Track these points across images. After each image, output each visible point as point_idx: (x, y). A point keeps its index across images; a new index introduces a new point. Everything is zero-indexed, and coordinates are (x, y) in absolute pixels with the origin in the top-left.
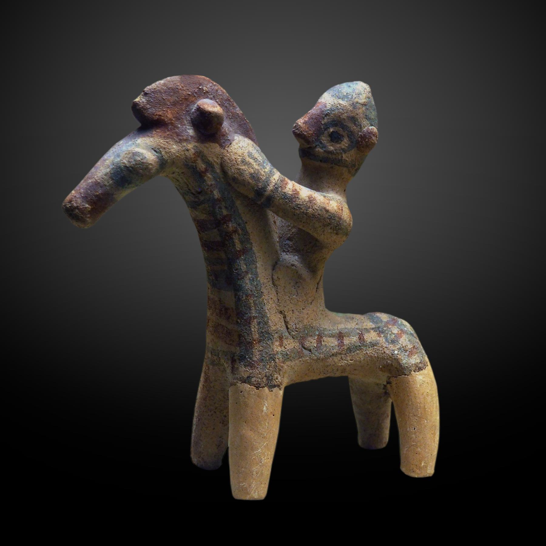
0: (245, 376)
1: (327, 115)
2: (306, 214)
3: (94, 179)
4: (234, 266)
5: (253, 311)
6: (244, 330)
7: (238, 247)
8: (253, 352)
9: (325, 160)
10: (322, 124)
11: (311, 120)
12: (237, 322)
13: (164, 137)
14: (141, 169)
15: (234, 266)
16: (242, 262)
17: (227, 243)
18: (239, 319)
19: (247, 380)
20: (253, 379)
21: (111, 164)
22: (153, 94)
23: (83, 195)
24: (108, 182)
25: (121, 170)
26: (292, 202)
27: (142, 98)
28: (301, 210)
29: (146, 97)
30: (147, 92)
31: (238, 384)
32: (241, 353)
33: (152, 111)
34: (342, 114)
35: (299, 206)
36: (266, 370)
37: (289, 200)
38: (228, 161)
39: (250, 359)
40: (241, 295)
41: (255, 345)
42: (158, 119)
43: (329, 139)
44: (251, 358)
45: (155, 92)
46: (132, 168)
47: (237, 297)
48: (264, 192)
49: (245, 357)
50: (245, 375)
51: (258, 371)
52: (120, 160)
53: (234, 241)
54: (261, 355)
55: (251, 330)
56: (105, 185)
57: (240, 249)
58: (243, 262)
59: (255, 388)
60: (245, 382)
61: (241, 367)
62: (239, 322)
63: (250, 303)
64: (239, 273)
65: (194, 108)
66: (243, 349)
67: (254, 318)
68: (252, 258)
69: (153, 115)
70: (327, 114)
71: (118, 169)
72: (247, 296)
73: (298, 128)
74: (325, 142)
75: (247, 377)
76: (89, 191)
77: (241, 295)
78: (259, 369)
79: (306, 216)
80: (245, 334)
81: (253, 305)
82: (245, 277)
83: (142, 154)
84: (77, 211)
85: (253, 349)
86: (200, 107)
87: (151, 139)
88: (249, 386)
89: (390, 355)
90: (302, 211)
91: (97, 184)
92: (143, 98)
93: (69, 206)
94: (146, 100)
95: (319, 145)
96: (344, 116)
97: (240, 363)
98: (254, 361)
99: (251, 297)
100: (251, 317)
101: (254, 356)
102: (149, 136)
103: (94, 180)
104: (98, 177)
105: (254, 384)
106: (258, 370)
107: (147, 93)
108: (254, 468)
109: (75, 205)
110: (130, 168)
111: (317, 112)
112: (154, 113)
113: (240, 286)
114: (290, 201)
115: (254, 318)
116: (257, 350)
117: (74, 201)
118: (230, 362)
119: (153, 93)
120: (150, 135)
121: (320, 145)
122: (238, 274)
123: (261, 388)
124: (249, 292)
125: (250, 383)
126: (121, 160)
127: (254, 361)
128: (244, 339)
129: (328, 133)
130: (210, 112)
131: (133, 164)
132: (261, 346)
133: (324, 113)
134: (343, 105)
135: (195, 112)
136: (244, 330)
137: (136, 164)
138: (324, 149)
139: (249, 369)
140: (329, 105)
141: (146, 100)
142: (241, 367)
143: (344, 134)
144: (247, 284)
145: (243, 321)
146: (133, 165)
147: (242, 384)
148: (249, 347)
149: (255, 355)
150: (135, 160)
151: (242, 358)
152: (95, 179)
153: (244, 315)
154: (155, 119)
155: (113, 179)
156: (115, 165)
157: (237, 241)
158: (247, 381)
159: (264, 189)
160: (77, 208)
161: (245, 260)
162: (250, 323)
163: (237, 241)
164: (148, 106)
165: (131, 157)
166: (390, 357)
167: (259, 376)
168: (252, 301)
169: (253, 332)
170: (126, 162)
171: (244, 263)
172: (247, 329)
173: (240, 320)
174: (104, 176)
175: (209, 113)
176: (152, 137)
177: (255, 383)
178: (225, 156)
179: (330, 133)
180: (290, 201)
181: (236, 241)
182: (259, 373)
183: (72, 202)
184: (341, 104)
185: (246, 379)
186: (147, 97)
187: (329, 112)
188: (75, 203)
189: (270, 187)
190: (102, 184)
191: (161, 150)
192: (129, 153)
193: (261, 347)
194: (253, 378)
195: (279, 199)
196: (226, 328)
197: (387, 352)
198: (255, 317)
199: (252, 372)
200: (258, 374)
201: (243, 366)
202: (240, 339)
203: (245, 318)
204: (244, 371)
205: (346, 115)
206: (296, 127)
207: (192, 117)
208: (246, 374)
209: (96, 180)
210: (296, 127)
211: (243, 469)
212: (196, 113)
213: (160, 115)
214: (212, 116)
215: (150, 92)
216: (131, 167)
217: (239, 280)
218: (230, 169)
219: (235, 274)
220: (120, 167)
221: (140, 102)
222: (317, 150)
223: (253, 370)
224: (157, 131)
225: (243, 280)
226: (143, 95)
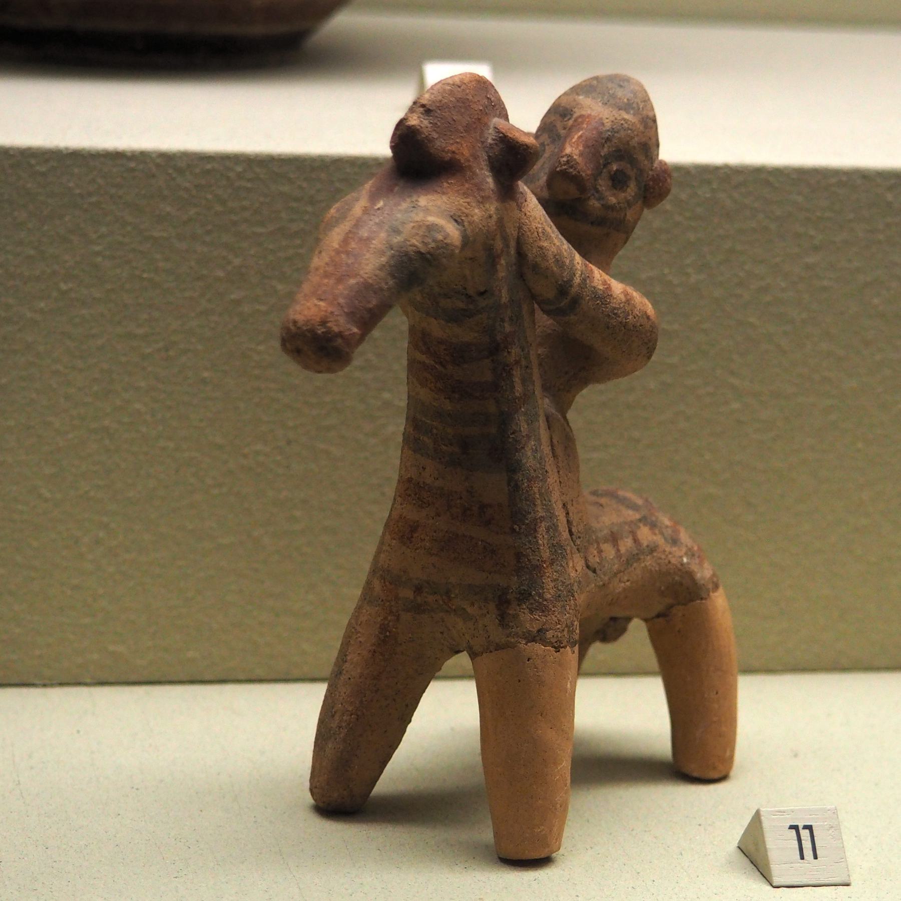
0: (535, 630)
1: (608, 139)
2: (625, 325)
3: (358, 277)
4: (510, 427)
5: (539, 508)
6: (527, 544)
7: (519, 389)
8: (543, 583)
9: (601, 222)
10: (601, 156)
11: (587, 150)
12: (513, 530)
13: (464, 194)
14: (445, 257)
15: (511, 426)
16: (522, 418)
17: (503, 383)
18: (516, 524)
19: (538, 636)
20: (549, 634)
21: (386, 247)
22: (439, 111)
23: (346, 310)
24: (387, 283)
25: (410, 259)
26: (606, 304)
27: (422, 120)
28: (617, 319)
29: (429, 116)
30: (431, 108)
31: (521, 646)
32: (522, 587)
33: (440, 143)
34: (632, 138)
35: (616, 311)
36: (565, 614)
37: (601, 301)
38: (529, 233)
39: (539, 597)
40: (520, 479)
41: (546, 571)
42: (451, 159)
43: (610, 183)
44: (541, 595)
45: (442, 106)
46: (431, 255)
47: (512, 484)
48: (569, 288)
49: (530, 594)
50: (533, 628)
51: (556, 618)
52: (402, 240)
53: (514, 380)
54: (557, 587)
55: (538, 542)
56: (381, 289)
57: (520, 394)
58: (523, 418)
59: (554, 649)
60: (534, 640)
61: (524, 613)
62: (518, 530)
63: (535, 493)
64: (518, 439)
65: (490, 137)
66: (527, 579)
67: (541, 520)
68: (535, 410)
69: (443, 151)
70: (607, 138)
71: (404, 258)
72: (529, 480)
73: (572, 165)
74: (603, 190)
75: (539, 631)
76: (357, 301)
77: (520, 479)
78: (556, 614)
79: (625, 329)
80: (528, 551)
81: (538, 496)
82: (526, 446)
83: (442, 227)
84: (340, 341)
85: (544, 577)
86: (508, 136)
87: (445, 198)
88: (543, 647)
89: (679, 566)
90: (620, 319)
91: (367, 286)
92: (424, 119)
93: (323, 332)
94: (431, 123)
95: (593, 195)
96: (634, 142)
97: (519, 605)
98: (546, 600)
99: (535, 481)
100: (537, 519)
101: (545, 590)
102: (439, 193)
103: (362, 280)
104: (366, 273)
105: (552, 644)
106: (556, 616)
107: (429, 109)
108: (558, 798)
109: (336, 329)
110: (428, 256)
111: (593, 134)
112: (445, 148)
113: (519, 462)
114: (602, 304)
115: (541, 520)
116: (549, 579)
117: (331, 321)
118: (492, 606)
119: (440, 110)
120: (439, 189)
121: (595, 194)
122: (516, 441)
123: (562, 648)
124: (533, 474)
125: (544, 642)
126: (406, 240)
127: (546, 600)
128: (526, 560)
129: (609, 172)
130: (527, 145)
131: (432, 248)
132: (555, 572)
133: (603, 136)
134: (631, 121)
135: (496, 144)
136: (527, 544)
137: (438, 248)
138: (602, 202)
139: (539, 616)
140: (607, 120)
141: (431, 123)
142: (524, 613)
143: (632, 173)
144: (528, 459)
145: (524, 526)
146: (432, 250)
147: (529, 644)
148: (537, 575)
149: (547, 589)
150: (435, 241)
151: (524, 596)
152: (363, 278)
153: (525, 516)
154: (446, 159)
155: (394, 276)
156: (394, 249)
157: (517, 379)
158: (538, 638)
159: (569, 283)
160: (340, 335)
161: (525, 414)
162: (535, 531)
163: (517, 379)
164: (435, 135)
165: (426, 234)
166: (680, 570)
167: (558, 627)
168: (536, 490)
169: (541, 546)
170: (416, 243)
171: (525, 420)
172: (532, 541)
173: (518, 525)
174: (378, 271)
175: (525, 147)
176: (444, 193)
177: (553, 640)
178: (524, 224)
179: (612, 173)
180: (602, 304)
181: (517, 380)
182: (557, 621)
183: (329, 325)
184: (628, 120)
185: (536, 635)
186: (431, 118)
187: (610, 133)
188: (335, 325)
189: (577, 280)
190: (377, 287)
191: (463, 218)
192: (420, 226)
193: (555, 574)
194: (548, 631)
195: (589, 300)
196: (482, 541)
197: (673, 561)
198: (542, 519)
199: (546, 620)
200: (556, 622)
201: (526, 611)
202: (518, 562)
203: (526, 521)
204: (529, 620)
205: (636, 139)
206: (569, 164)
207: (491, 154)
208: (535, 626)
209: (365, 280)
210: (569, 164)
211: (540, 802)
212: (498, 146)
213: (454, 152)
214: (530, 152)
215: (434, 108)
216: (429, 253)
217: (517, 452)
218: (530, 247)
219: (511, 440)
220: (406, 254)
221: (421, 127)
222: (591, 204)
223: (547, 617)
224: (450, 181)
225: (523, 450)
226: (424, 112)
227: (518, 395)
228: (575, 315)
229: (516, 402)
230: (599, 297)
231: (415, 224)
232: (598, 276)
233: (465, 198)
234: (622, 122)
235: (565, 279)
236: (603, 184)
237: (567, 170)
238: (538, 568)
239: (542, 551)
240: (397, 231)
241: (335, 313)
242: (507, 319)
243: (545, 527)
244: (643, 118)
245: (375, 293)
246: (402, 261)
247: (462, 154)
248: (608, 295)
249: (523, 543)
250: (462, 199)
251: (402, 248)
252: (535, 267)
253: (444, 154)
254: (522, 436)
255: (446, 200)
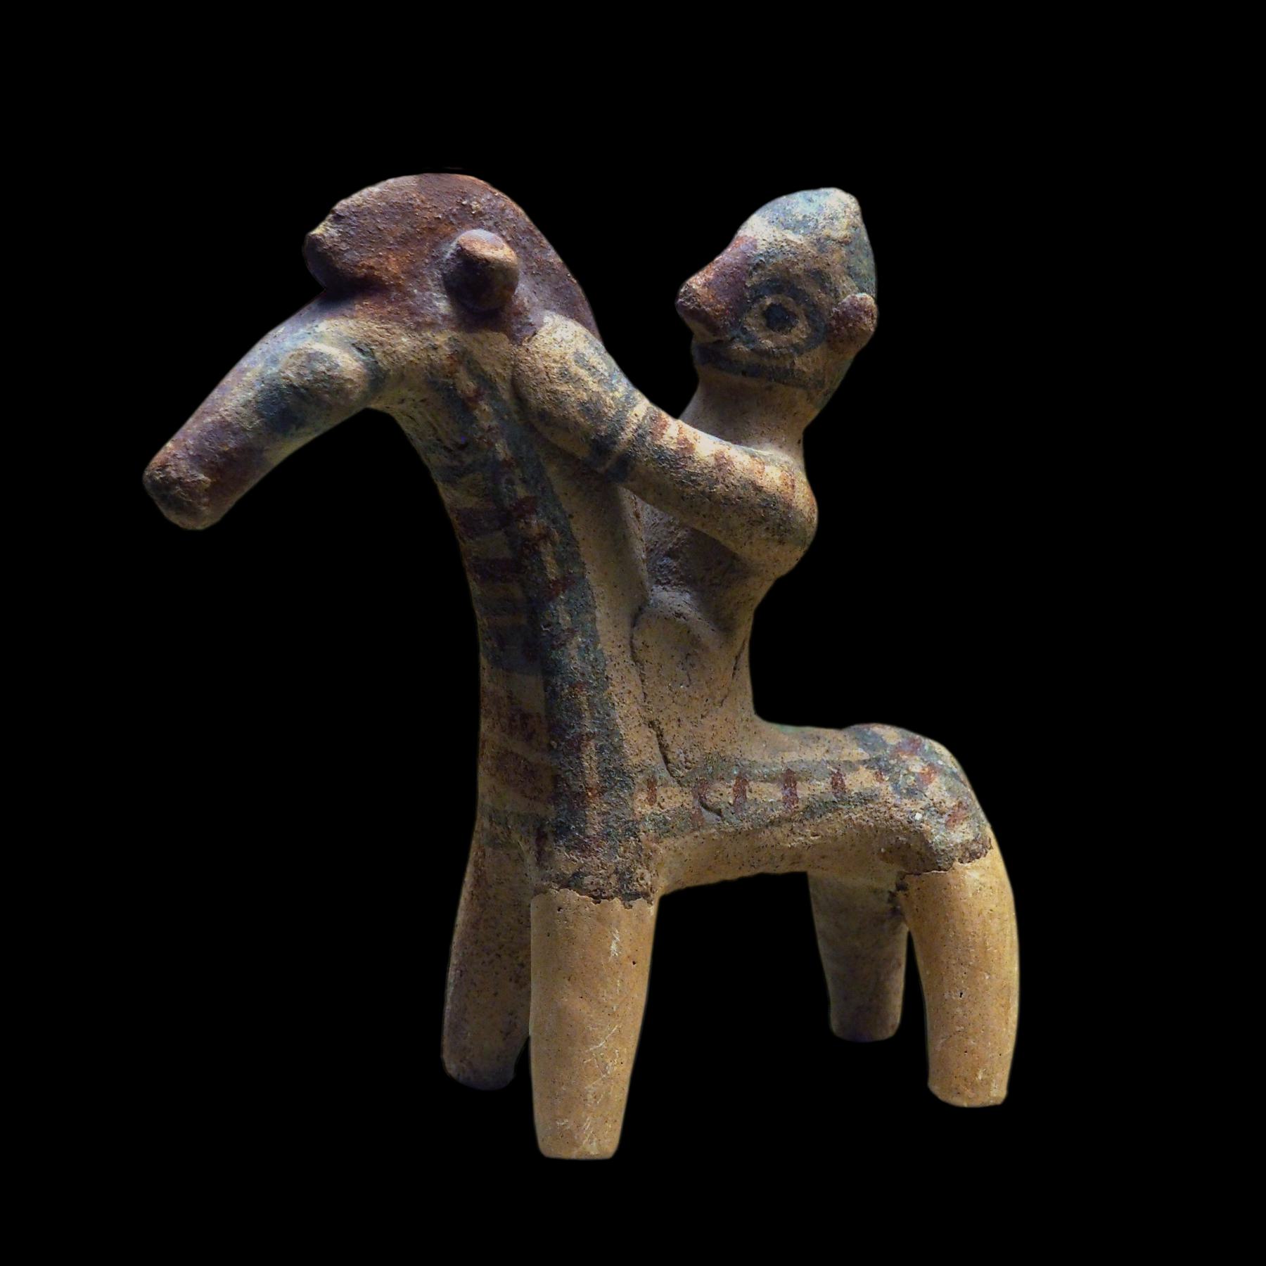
0: (569, 873)
1: (758, 266)
2: (710, 496)
3: (217, 414)
4: (542, 618)
5: (587, 722)
6: (567, 765)
7: (553, 572)
8: (586, 815)
9: (753, 371)
10: (746, 287)
11: (722, 279)
12: (550, 746)
13: (381, 318)
14: (328, 393)
15: (544, 617)
16: (561, 608)
17: (526, 562)
18: (553, 740)
19: (573, 882)
20: (587, 880)
21: (257, 380)
22: (355, 218)
23: (191, 453)
25: (281, 393)
26: (678, 468)
27: (328, 228)
28: (697, 487)
29: (339, 224)
30: (342, 214)
31: (552, 891)
33: (351, 256)
34: (794, 264)
38: (530, 373)
39: (580, 833)
40: (559, 684)
41: (591, 801)
42: (366, 276)
43: (763, 322)
44: (581, 831)
45: (360, 212)
46: (307, 389)
47: (550, 688)
48: (612, 446)
49: (568, 828)
50: (568, 870)
51: (599, 861)
52: (277, 371)
53: (544, 559)
54: (606, 823)
55: (582, 764)
57: (556, 578)
58: (563, 607)
59: (592, 899)
60: (567, 886)
61: (559, 851)
62: (555, 747)
63: (581, 703)
65: (449, 250)
66: (564, 809)
67: (588, 737)
68: (584, 599)
69: (356, 266)
70: (757, 264)
71: (274, 392)
72: (572, 686)
73: (690, 297)
74: (753, 330)
75: (574, 875)
76: (207, 443)
77: (559, 684)
78: (600, 855)
79: (710, 500)
80: (567, 773)
81: (586, 707)
84: (178, 488)
85: (588, 809)
86: (465, 249)
87: (351, 323)
88: (578, 895)
89: (905, 822)
90: (700, 488)
92: (331, 227)
94: (339, 232)
95: (739, 337)
96: (798, 269)
97: (556, 841)
98: (588, 837)
99: (581, 688)
100: (583, 735)
101: (588, 825)
102: (346, 316)
104: (226, 410)
105: (590, 891)
106: (598, 859)
107: (340, 216)
108: (589, 1086)
110: (302, 390)
111: (735, 259)
112: (358, 262)
113: (557, 663)
115: (588, 737)
116: (595, 812)
117: (170, 465)
119: (356, 216)
120: (347, 312)
121: (742, 335)
122: (553, 636)
123: (604, 899)
124: (578, 677)
125: (580, 889)
126: (280, 371)
127: (588, 837)
128: (565, 785)
129: (761, 308)
130: (486, 260)
131: (308, 380)
132: (606, 803)
133: (752, 261)
134: (796, 243)
135: (452, 259)
136: (567, 765)
137: (316, 381)
138: (752, 346)
139: (577, 856)
140: (764, 242)
141: (339, 232)
142: (559, 851)
144: (573, 658)
145: (563, 743)
146: (307, 383)
147: (561, 890)
148: (578, 805)
149: (591, 824)
150: (312, 372)
151: (561, 830)
152: (221, 416)
153: (565, 730)
154: (358, 276)
155: (261, 414)
156: (266, 382)
157: (549, 558)
158: (572, 884)
159: (612, 437)
160: (179, 481)
161: (567, 602)
162: (579, 750)
163: (549, 558)
164: (344, 246)
166: (905, 829)
167: (600, 872)
168: (583, 699)
170: (291, 375)
171: (566, 611)
172: (574, 762)
174: (241, 408)
175: (484, 262)
176: (352, 317)
177: (591, 888)
178: (522, 362)
179: (765, 309)
180: (671, 467)
182: (600, 865)
184: (792, 242)
185: (571, 879)
186: (341, 225)
187: (763, 259)
189: (627, 435)
190: (238, 426)
191: (373, 347)
192: (300, 355)
194: (586, 876)
195: (648, 461)
196: (525, 760)
198: (591, 736)
199: (585, 863)
200: (598, 866)
201: (563, 849)
202: (556, 787)
203: (567, 737)
204: (565, 860)
205: (801, 266)
206: (686, 295)
207: (445, 272)
208: (570, 868)
211: (564, 1088)
212: (455, 262)
213: (372, 268)
214: (491, 268)
215: (347, 214)
216: (303, 387)
217: (554, 649)
219: (544, 634)
220: (278, 388)
221: (324, 237)
223: (586, 858)
224: (364, 303)
225: (563, 649)
227: (554, 578)
228: (632, 480)
229: (549, 587)
230: (667, 459)
231: (294, 353)
232: (675, 431)
233: (383, 323)
234: (784, 244)
235: (603, 434)
236: (752, 323)
237: (684, 304)
238: (579, 799)
239: (587, 775)
240: (275, 361)
241: (179, 457)
242: (517, 481)
243: (595, 747)
244: (818, 240)
245: (235, 434)
246: (271, 396)
247: (387, 269)
248: (684, 457)
249: (561, 764)
250: (376, 324)
251: (274, 380)
252: (543, 415)
253: (356, 270)
254: (562, 630)
255: (352, 326)
